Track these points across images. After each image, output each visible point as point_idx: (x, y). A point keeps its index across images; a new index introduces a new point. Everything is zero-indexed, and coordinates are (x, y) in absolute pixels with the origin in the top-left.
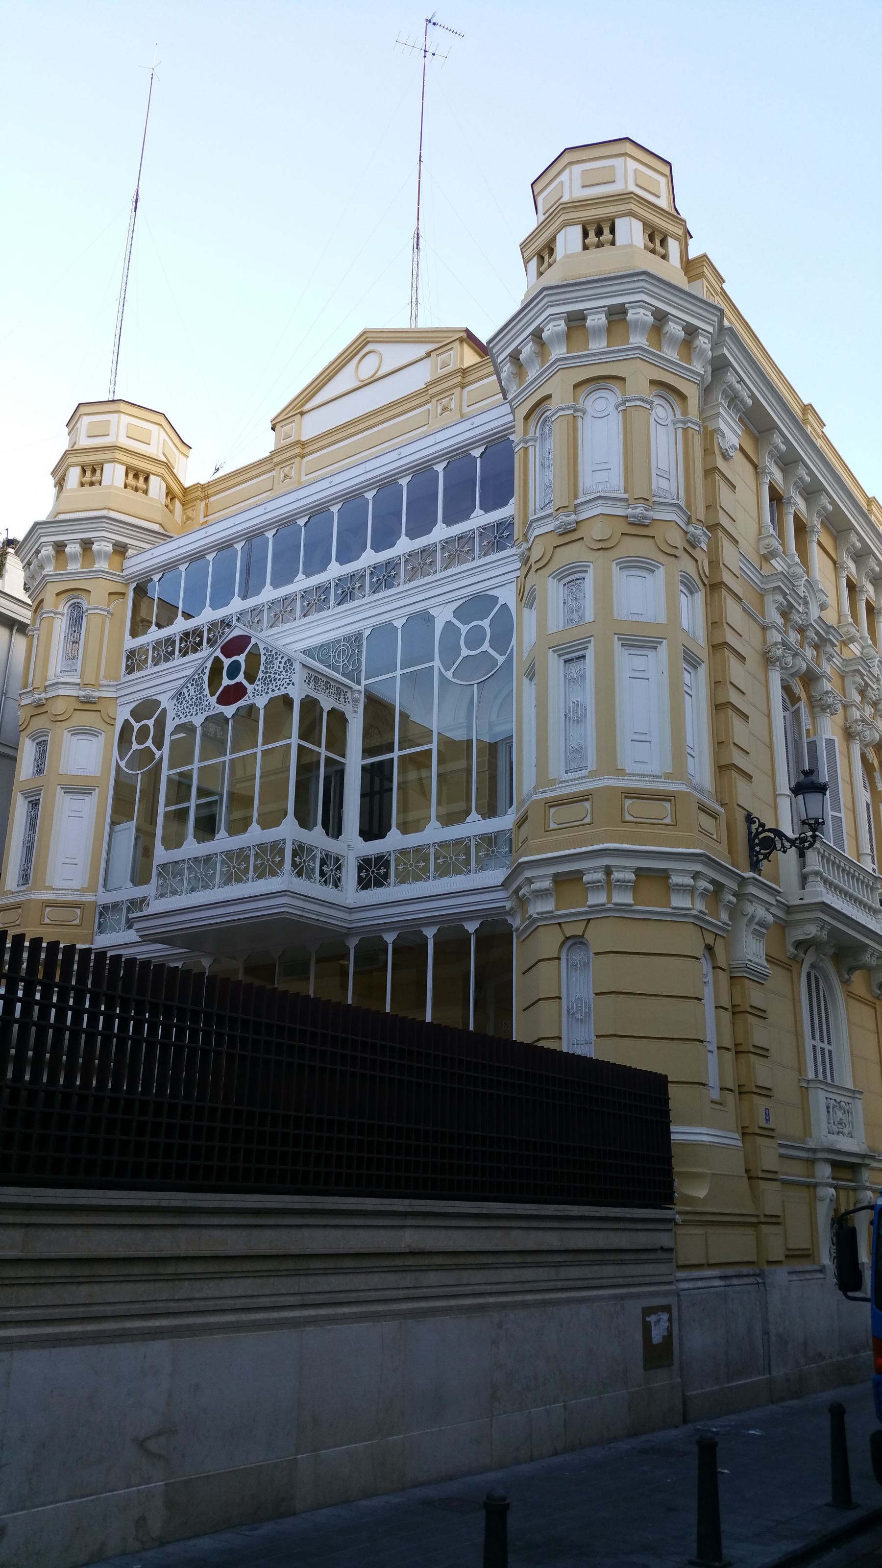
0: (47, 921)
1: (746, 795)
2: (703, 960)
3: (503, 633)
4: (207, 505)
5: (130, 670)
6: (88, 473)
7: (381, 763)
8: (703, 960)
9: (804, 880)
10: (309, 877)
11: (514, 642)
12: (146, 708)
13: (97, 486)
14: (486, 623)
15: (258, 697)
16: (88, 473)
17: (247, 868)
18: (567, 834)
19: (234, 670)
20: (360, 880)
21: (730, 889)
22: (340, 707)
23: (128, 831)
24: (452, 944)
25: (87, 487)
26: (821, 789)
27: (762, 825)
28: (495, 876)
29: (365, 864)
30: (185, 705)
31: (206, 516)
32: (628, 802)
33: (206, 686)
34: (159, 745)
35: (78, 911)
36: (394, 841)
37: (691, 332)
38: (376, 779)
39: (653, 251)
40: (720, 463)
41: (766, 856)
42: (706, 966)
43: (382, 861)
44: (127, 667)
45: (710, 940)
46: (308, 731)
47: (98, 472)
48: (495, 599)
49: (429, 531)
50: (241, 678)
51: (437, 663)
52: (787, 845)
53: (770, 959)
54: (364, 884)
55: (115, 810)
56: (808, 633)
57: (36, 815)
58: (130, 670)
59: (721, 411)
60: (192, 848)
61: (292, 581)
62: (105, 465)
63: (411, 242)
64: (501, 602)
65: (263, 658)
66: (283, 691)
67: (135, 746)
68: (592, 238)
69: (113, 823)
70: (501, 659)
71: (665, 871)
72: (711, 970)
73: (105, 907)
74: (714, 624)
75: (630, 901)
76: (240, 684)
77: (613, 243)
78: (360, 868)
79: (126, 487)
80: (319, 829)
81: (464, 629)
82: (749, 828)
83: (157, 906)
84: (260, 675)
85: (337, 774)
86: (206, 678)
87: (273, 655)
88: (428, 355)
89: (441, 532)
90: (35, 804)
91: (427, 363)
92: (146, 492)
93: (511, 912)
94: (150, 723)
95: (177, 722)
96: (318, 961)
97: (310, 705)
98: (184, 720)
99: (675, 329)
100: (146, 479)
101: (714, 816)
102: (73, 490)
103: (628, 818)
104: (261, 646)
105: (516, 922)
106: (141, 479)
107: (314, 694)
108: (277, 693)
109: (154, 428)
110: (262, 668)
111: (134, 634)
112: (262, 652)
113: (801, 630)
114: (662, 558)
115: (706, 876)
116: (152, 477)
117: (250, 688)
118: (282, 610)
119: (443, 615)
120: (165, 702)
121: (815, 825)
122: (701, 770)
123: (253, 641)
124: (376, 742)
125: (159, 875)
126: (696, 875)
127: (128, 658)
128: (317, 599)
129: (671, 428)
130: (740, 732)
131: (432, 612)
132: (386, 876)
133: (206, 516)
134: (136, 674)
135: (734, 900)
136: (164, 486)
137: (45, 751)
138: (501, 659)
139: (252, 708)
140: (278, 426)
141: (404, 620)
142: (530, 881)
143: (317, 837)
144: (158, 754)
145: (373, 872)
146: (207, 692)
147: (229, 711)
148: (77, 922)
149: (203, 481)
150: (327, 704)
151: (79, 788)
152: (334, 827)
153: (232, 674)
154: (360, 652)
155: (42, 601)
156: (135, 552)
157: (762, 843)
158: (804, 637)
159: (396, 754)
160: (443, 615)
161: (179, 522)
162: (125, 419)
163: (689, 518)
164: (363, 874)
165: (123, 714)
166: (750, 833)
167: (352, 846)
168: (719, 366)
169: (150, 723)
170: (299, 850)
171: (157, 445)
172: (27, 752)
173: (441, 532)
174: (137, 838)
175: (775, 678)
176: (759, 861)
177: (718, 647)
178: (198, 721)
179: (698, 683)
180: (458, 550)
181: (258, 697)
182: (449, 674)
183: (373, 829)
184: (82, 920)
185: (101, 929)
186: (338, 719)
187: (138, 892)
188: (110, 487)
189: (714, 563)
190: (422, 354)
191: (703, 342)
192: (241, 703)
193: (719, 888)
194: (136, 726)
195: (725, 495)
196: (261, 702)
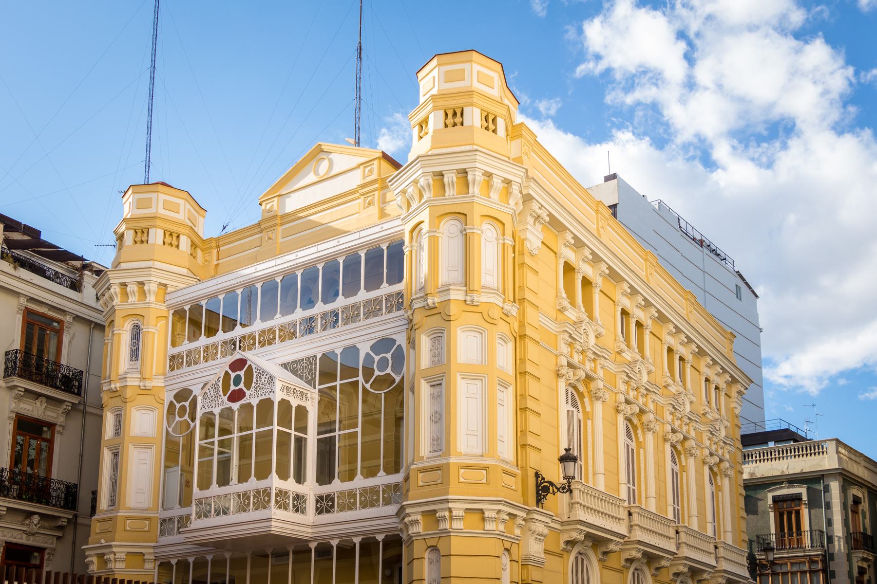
0: (128, 528)
1: (534, 460)
2: (503, 557)
3: (399, 359)
4: (218, 252)
5: (172, 369)
6: (139, 234)
7: (330, 437)
8: (503, 557)
9: (571, 505)
10: (286, 509)
11: (405, 369)
12: (183, 395)
13: (145, 244)
14: (389, 356)
15: (253, 399)
16: (139, 234)
17: (249, 504)
18: (427, 489)
19: (237, 380)
20: (317, 508)
21: (521, 517)
22: (302, 403)
23: (176, 472)
24: (368, 546)
25: (138, 244)
26: (574, 459)
27: (543, 479)
28: (392, 509)
29: (320, 499)
30: (208, 400)
31: (218, 260)
32: (462, 471)
33: (220, 389)
34: (193, 419)
35: (147, 522)
36: (337, 486)
37: (508, 182)
38: (326, 449)
39: (487, 128)
40: (528, 260)
41: (545, 497)
42: (506, 559)
43: (329, 498)
44: (170, 366)
45: (508, 545)
46: (284, 420)
47: (146, 233)
48: (394, 341)
49: (356, 294)
50: (242, 386)
51: (361, 378)
52: (556, 490)
53: (546, 552)
54: (319, 511)
55: (167, 459)
56: (588, 354)
57: (117, 462)
58: (172, 369)
59: (529, 227)
60: (215, 489)
61: (273, 318)
62: (150, 230)
63: (356, 54)
64: (398, 343)
65: (255, 374)
66: (267, 396)
67: (177, 419)
68: (450, 121)
69: (166, 467)
70: (398, 379)
71: (482, 510)
72: (509, 562)
73: (164, 520)
74: (520, 361)
75: (462, 527)
76: (241, 390)
77: (462, 124)
78: (317, 501)
79: (164, 244)
80: (291, 480)
81: (377, 358)
82: (537, 480)
83: (196, 523)
84: (253, 385)
85: (300, 443)
86: (220, 384)
87: (262, 372)
88: (358, 166)
89: (363, 295)
90: (116, 455)
91: (359, 172)
92: (178, 246)
93: (401, 530)
94: (187, 404)
95: (204, 411)
96: (294, 553)
97: (285, 405)
98: (208, 410)
99: (497, 182)
100: (178, 237)
101: (513, 475)
102: (129, 246)
103: (462, 480)
104: (254, 367)
105: (404, 537)
106: (174, 238)
107: (286, 398)
108: (264, 397)
109: (181, 202)
110: (254, 380)
111: (174, 344)
112: (254, 370)
113: (583, 352)
114: (487, 325)
115: (504, 512)
116: (181, 236)
117: (247, 393)
118: (267, 339)
119: (364, 349)
120: (197, 391)
121: (569, 479)
122: (507, 450)
123: (249, 363)
124: (326, 420)
125: (197, 505)
126: (499, 511)
127: (171, 360)
128: (288, 333)
129: (495, 242)
130: (533, 423)
131: (358, 346)
132: (333, 506)
133: (218, 260)
134: (176, 372)
135: (523, 523)
136: (189, 241)
137: (120, 421)
138: (398, 379)
139: (250, 406)
140: (264, 204)
141: (341, 350)
142: (408, 515)
143: (290, 485)
144: (192, 424)
145: (325, 504)
146: (221, 393)
147: (236, 406)
148: (147, 529)
149: (215, 236)
150: (295, 402)
151: (143, 443)
152: (300, 478)
153: (236, 383)
154: (315, 368)
155: (113, 321)
156: (173, 290)
157: (543, 489)
158: (585, 357)
159: (337, 433)
160: (364, 349)
161: (201, 264)
162: (162, 197)
163: (504, 299)
164: (319, 505)
165: (168, 397)
166: (537, 483)
167: (311, 488)
168: (527, 199)
169: (187, 404)
170: (281, 493)
171: (183, 212)
172: (109, 420)
173: (363, 295)
174: (181, 475)
175: (562, 385)
176: (541, 500)
177: (521, 373)
178: (217, 411)
179: (507, 398)
180: (373, 308)
181: (253, 399)
182: (368, 386)
183: (325, 475)
184: (150, 527)
185: (162, 533)
186: (302, 412)
187: (184, 511)
188: (154, 245)
189: (522, 325)
190: (354, 165)
191: (515, 188)
192: (242, 402)
193: (512, 516)
194: (178, 406)
195: (531, 280)
196: (255, 402)
